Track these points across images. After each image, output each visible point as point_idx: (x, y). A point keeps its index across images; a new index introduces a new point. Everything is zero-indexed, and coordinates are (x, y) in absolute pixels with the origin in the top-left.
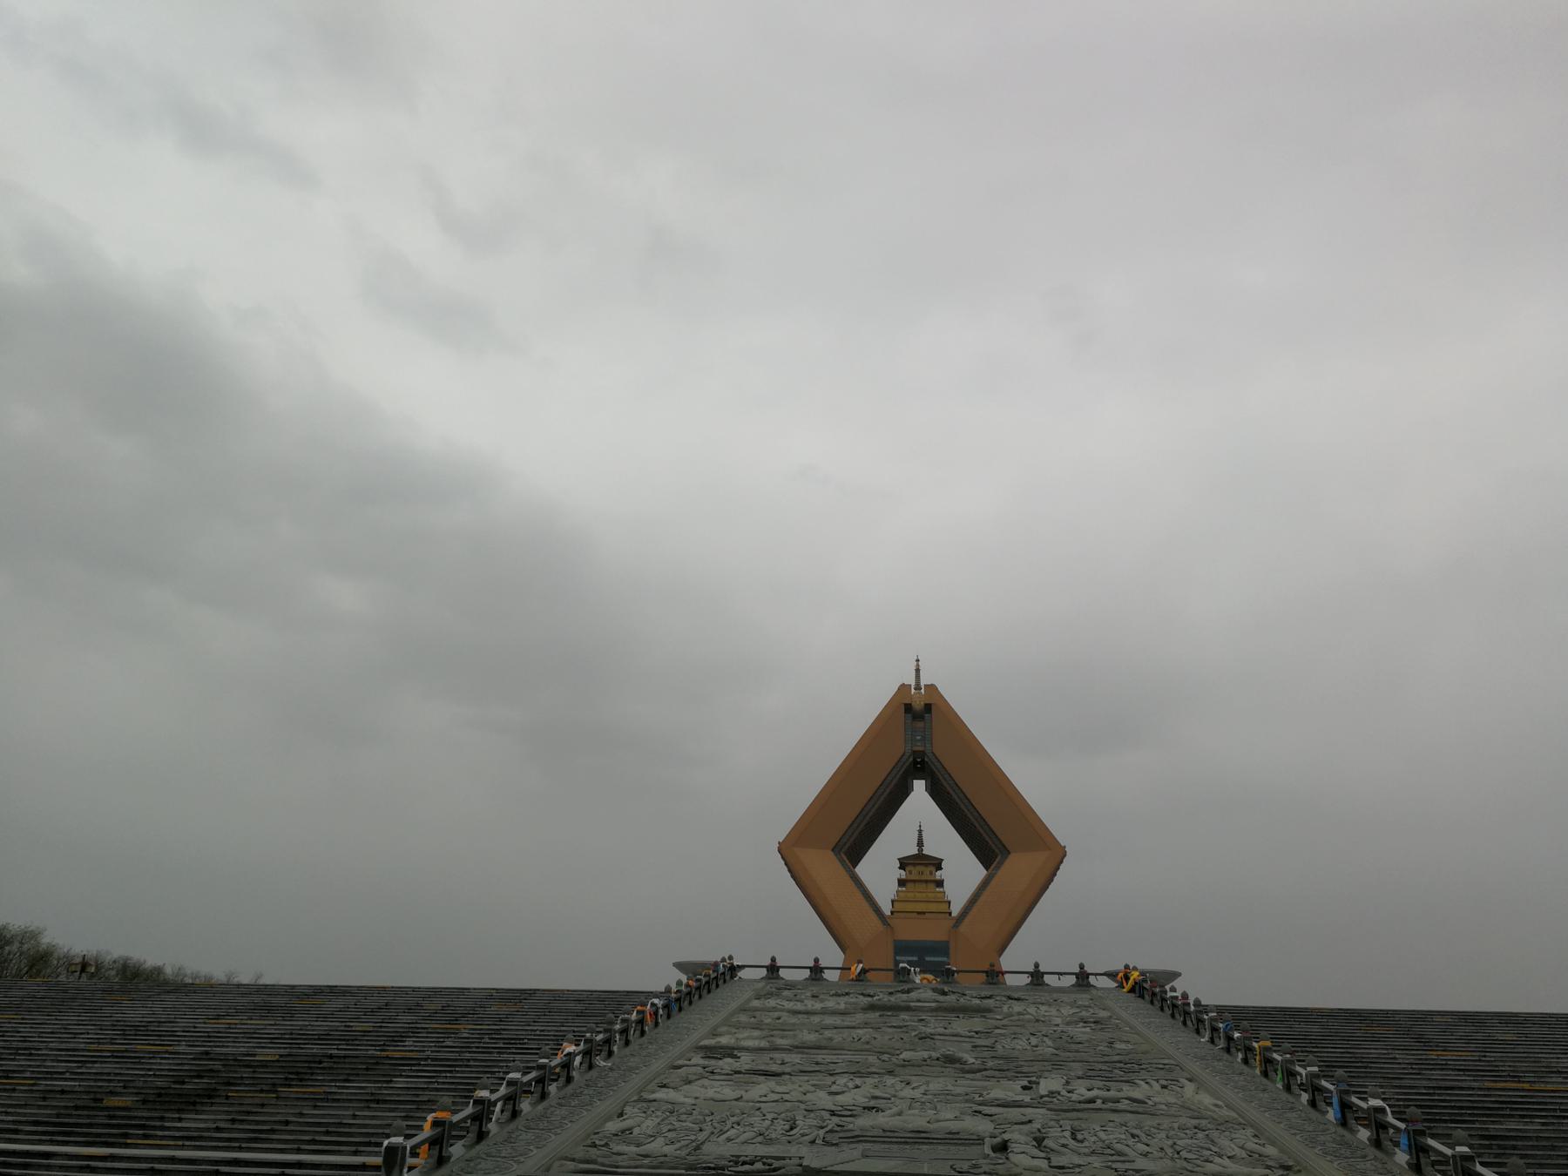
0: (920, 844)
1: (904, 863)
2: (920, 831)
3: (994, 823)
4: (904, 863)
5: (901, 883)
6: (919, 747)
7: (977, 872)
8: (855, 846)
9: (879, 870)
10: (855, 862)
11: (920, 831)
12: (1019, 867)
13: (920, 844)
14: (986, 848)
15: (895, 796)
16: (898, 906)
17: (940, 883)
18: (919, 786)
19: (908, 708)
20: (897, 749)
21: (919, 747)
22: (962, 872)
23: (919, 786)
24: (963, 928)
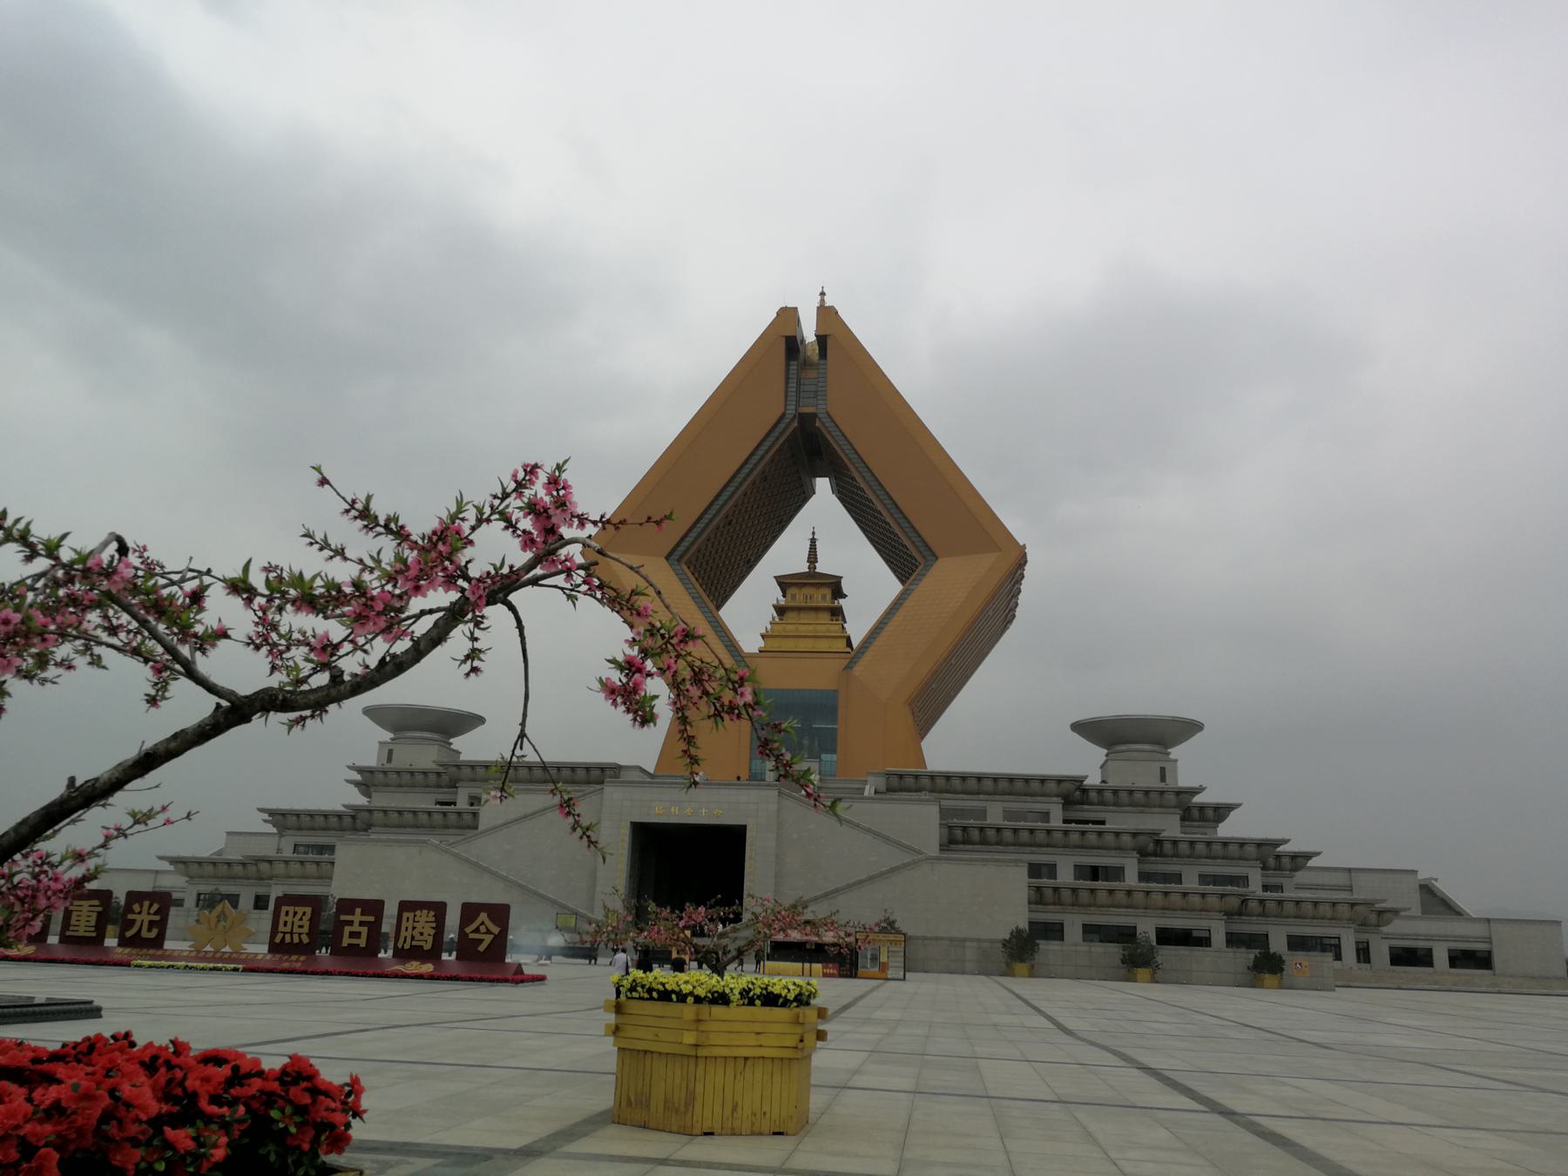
0: (813, 557)
1: (784, 583)
2: (813, 541)
3: (923, 514)
4: (784, 583)
5: (781, 610)
6: (805, 419)
7: (894, 586)
8: (718, 560)
9: (750, 612)
10: (721, 597)
11: (813, 541)
12: (955, 580)
13: (813, 557)
14: (902, 553)
15: (762, 503)
16: (775, 644)
17: (837, 613)
18: (823, 485)
19: (793, 345)
20: (770, 407)
21: (805, 419)
22: (869, 585)
23: (823, 485)
24: (858, 670)
